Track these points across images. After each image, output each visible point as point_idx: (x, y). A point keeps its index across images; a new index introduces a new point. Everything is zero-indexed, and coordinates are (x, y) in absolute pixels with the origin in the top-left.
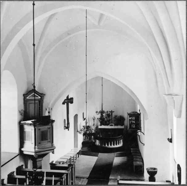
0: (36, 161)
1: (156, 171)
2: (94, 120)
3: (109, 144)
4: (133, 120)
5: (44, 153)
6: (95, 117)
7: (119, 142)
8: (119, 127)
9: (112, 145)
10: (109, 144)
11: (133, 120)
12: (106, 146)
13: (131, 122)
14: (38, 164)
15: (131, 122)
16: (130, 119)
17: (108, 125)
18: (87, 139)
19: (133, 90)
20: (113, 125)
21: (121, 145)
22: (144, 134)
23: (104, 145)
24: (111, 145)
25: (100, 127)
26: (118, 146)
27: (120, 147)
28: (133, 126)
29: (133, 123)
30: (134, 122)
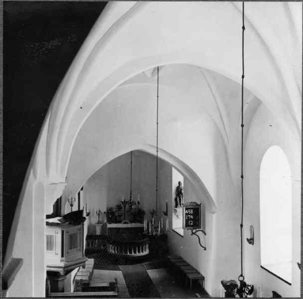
0: (58, 281)
1: (160, 291)
2: (99, 215)
3: (133, 252)
4: (191, 214)
5: (70, 268)
6: (101, 210)
7: (143, 247)
8: (133, 225)
9: (137, 253)
10: (133, 252)
11: (191, 214)
12: (129, 254)
13: (188, 217)
14: (60, 285)
15: (188, 217)
16: (186, 214)
17: (120, 222)
18: (92, 246)
19: (195, 170)
20: (128, 221)
21: (146, 252)
22: (205, 234)
23: (125, 253)
24: (135, 253)
25: (109, 226)
26: (142, 254)
27: (147, 255)
28: (191, 223)
29: (191, 219)
30: (192, 217)
